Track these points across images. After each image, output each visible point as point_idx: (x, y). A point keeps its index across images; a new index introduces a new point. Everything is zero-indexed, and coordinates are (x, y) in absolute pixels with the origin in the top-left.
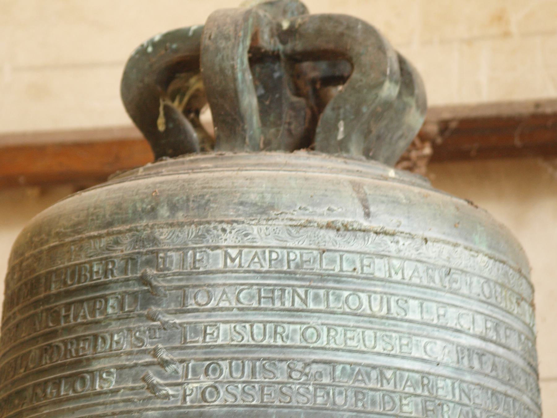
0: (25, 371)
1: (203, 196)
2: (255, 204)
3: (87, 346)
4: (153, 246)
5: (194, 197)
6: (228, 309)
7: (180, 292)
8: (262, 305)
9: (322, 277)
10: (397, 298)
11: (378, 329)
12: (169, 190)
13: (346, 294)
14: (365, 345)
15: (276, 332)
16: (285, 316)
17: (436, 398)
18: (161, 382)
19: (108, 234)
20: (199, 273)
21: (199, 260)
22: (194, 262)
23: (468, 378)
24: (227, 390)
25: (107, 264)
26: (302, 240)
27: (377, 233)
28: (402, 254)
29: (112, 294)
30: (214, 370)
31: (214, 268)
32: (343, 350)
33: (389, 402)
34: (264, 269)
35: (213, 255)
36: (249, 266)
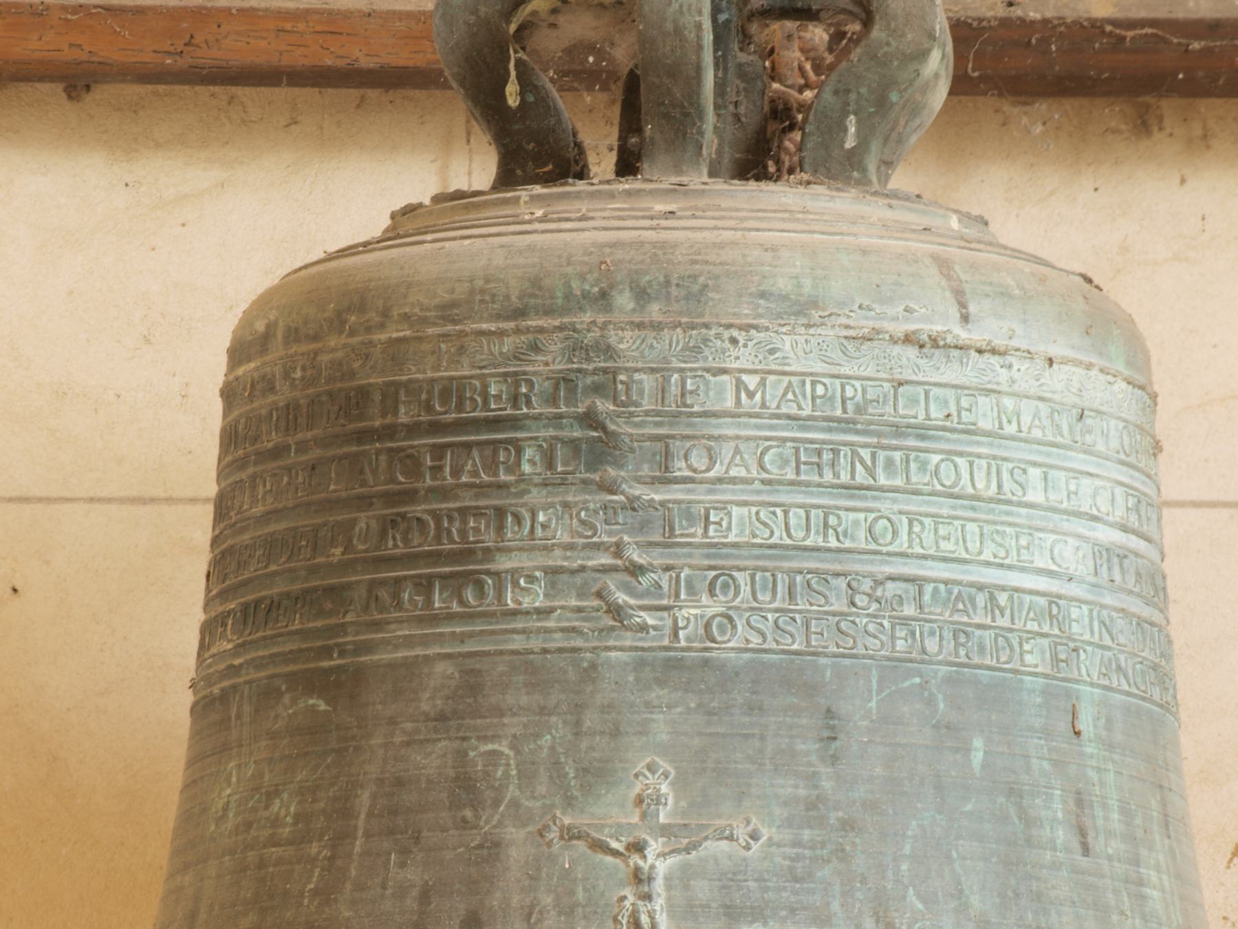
0: (343, 554)
1: (694, 277)
2: (784, 298)
3: (483, 527)
4: (605, 361)
5: (679, 278)
6: (744, 481)
7: (659, 446)
8: (803, 477)
9: (898, 430)
10: (1010, 465)
11: (984, 521)
12: (630, 262)
13: (935, 458)
14: (966, 549)
15: (826, 525)
16: (841, 496)
17: (1069, 638)
18: (632, 602)
19: (518, 331)
20: (691, 415)
21: (691, 392)
22: (683, 395)
23: (1108, 600)
24: (748, 623)
25: (517, 385)
26: (864, 364)
27: (980, 351)
28: (1016, 388)
29: (531, 438)
30: (725, 586)
31: (717, 408)
32: (933, 558)
33: (1004, 648)
34: (804, 413)
35: (716, 383)
36: (778, 407)
